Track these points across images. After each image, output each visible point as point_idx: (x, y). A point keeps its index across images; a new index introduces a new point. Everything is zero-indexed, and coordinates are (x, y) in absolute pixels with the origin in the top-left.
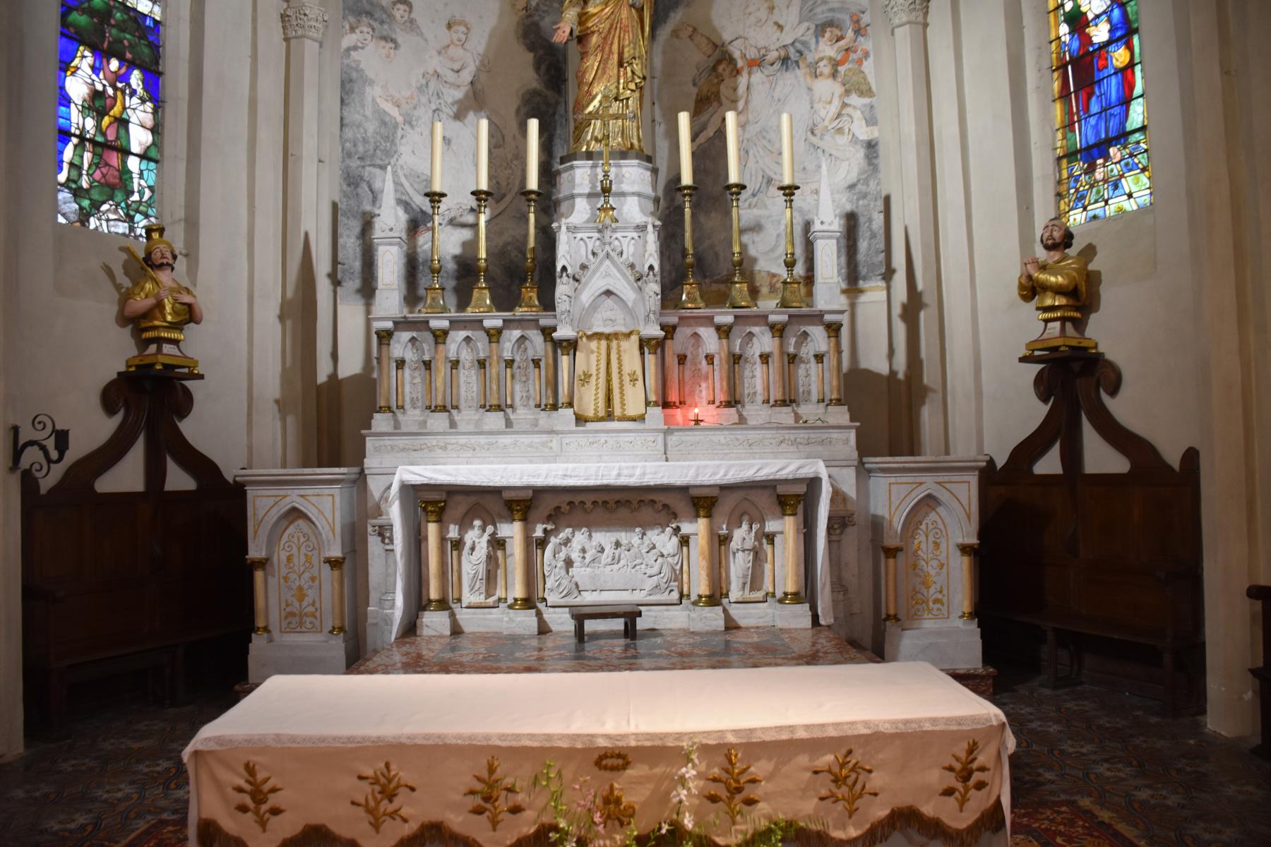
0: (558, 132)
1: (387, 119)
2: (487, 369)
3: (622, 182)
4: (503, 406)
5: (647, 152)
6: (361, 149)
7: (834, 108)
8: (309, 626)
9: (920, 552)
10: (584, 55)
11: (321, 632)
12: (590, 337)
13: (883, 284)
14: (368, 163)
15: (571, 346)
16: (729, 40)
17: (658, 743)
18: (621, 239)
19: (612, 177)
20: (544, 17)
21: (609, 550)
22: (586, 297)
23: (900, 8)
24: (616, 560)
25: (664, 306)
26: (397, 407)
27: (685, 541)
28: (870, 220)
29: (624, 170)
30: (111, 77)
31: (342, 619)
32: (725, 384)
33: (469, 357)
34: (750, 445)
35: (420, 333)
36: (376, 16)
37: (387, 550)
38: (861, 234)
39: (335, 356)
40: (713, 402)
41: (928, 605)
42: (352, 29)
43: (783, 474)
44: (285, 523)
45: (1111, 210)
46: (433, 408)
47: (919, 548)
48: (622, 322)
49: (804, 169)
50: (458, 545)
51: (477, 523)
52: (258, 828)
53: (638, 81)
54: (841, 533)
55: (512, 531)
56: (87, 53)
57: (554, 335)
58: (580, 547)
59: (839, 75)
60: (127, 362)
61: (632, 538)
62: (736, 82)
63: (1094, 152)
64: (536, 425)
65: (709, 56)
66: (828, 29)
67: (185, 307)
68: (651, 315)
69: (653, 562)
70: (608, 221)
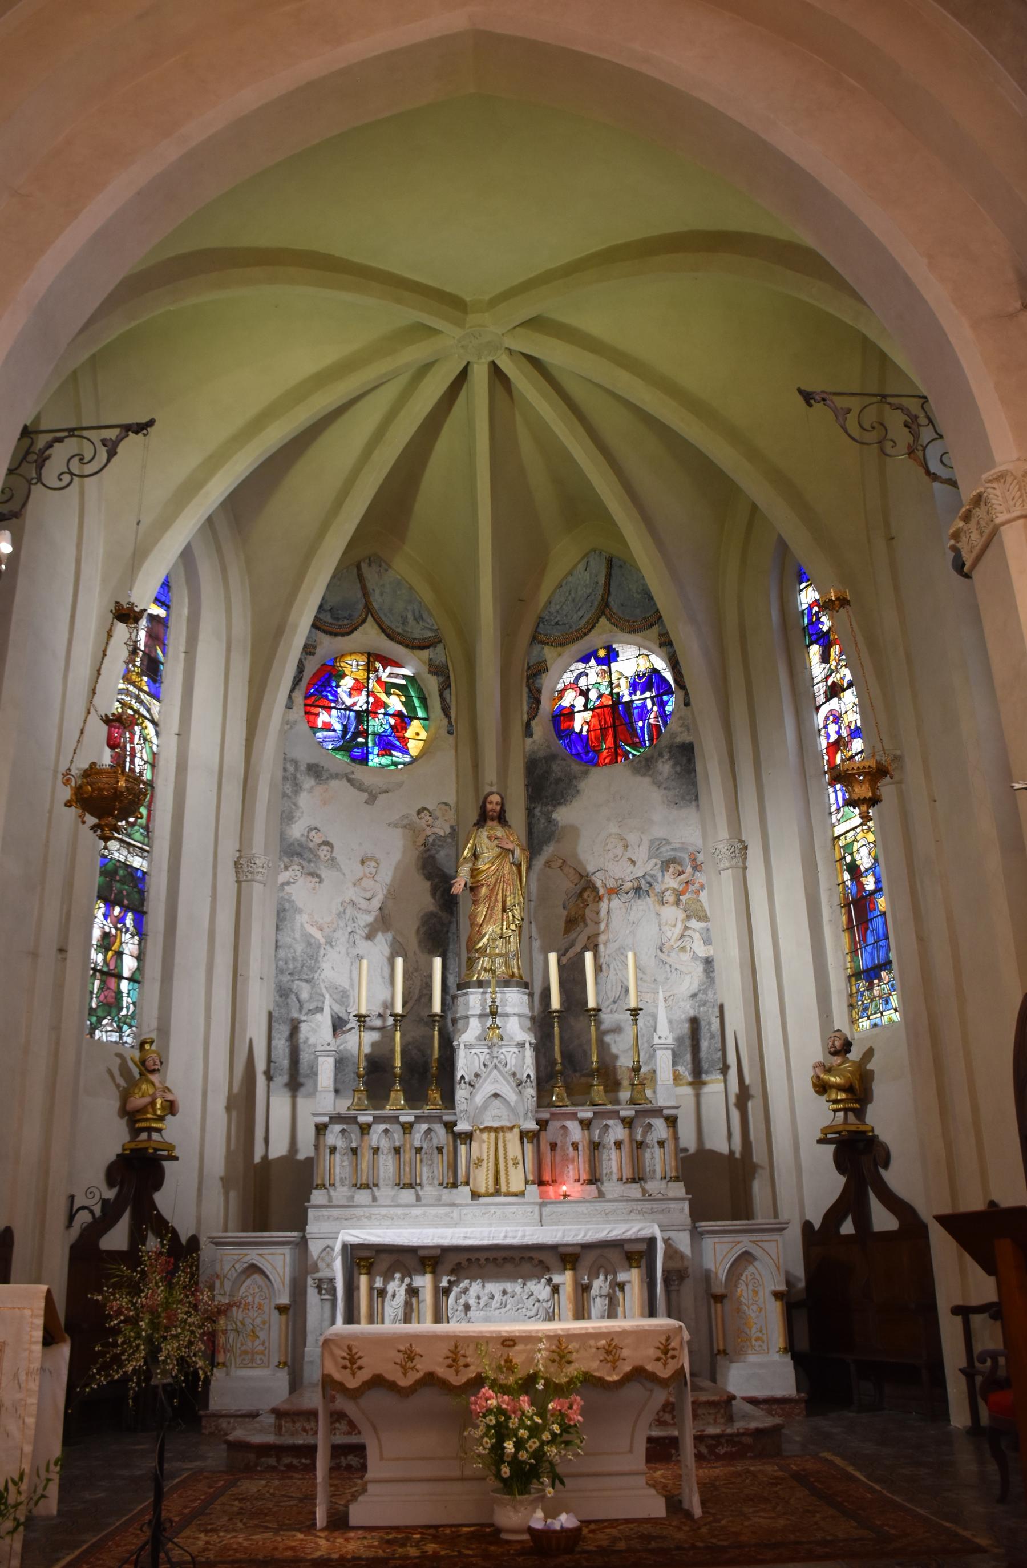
0: (451, 947)
1: (313, 941)
2: (402, 1154)
3: (506, 1005)
4: (414, 1184)
5: (526, 979)
6: (291, 966)
7: (678, 930)
8: (259, 1362)
9: (742, 1299)
10: (475, 902)
11: (268, 1367)
12: (482, 1130)
13: (721, 1077)
14: (297, 977)
15: (468, 1137)
16: (592, 871)
17: (528, 1334)
18: (506, 1053)
19: (498, 1000)
20: (439, 851)
21: (498, 1297)
22: (479, 1099)
23: (724, 856)
24: (503, 1305)
25: (539, 1105)
26: (330, 1185)
27: (556, 1289)
28: (709, 1024)
29: (508, 995)
30: (115, 920)
31: (287, 1357)
32: (587, 1166)
33: (387, 1145)
34: (606, 1214)
35: (349, 1126)
36: (305, 856)
37: (322, 1300)
38: (702, 1035)
39: (266, 1140)
40: (579, 1181)
41: (751, 1343)
42: (286, 868)
43: (629, 1235)
44: (244, 1277)
45: (885, 1020)
46: (358, 1186)
47: (741, 1295)
48: (507, 1117)
49: (655, 980)
50: (382, 1293)
51: (397, 1275)
52: (351, 1376)
53: (517, 922)
54: (680, 1284)
55: (424, 1282)
56: (102, 905)
57: (455, 1129)
58: (475, 1295)
59: (681, 903)
60: (123, 1146)
61: (515, 1287)
62: (598, 906)
63: (871, 974)
64: (440, 1200)
65: (576, 885)
66: (672, 865)
67: (168, 1103)
68: (529, 1113)
69: (531, 1306)
70: (495, 1040)
